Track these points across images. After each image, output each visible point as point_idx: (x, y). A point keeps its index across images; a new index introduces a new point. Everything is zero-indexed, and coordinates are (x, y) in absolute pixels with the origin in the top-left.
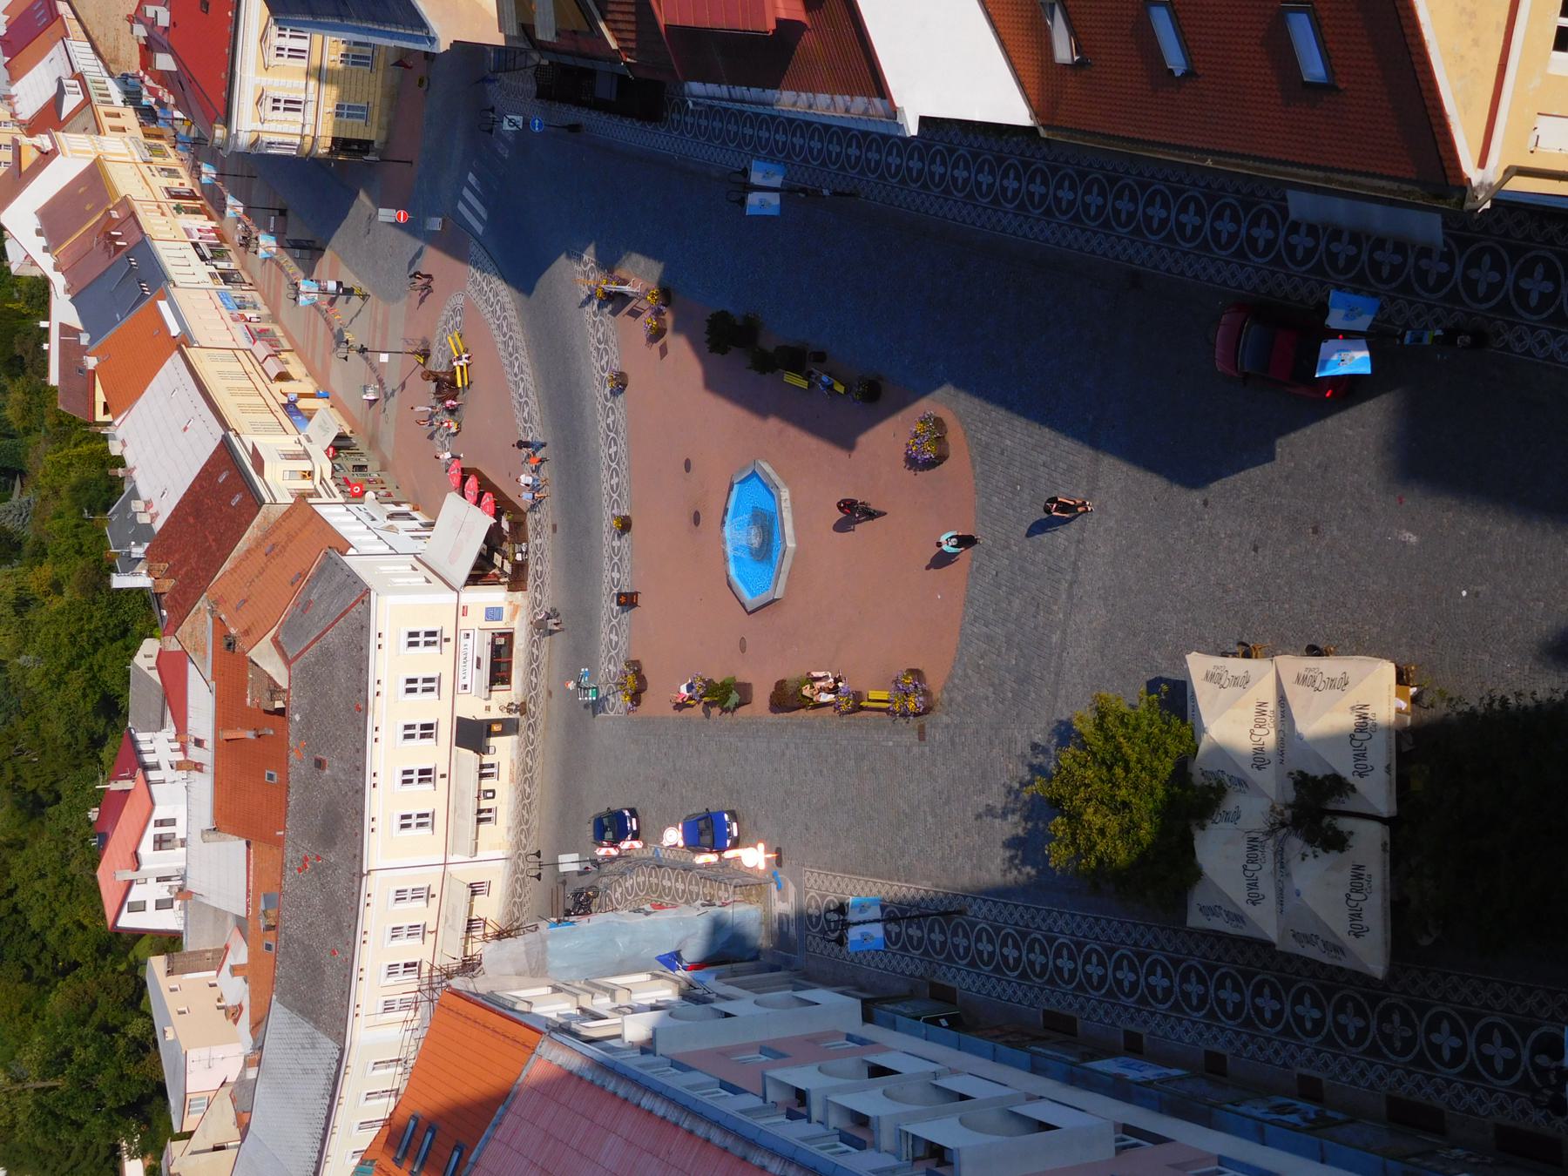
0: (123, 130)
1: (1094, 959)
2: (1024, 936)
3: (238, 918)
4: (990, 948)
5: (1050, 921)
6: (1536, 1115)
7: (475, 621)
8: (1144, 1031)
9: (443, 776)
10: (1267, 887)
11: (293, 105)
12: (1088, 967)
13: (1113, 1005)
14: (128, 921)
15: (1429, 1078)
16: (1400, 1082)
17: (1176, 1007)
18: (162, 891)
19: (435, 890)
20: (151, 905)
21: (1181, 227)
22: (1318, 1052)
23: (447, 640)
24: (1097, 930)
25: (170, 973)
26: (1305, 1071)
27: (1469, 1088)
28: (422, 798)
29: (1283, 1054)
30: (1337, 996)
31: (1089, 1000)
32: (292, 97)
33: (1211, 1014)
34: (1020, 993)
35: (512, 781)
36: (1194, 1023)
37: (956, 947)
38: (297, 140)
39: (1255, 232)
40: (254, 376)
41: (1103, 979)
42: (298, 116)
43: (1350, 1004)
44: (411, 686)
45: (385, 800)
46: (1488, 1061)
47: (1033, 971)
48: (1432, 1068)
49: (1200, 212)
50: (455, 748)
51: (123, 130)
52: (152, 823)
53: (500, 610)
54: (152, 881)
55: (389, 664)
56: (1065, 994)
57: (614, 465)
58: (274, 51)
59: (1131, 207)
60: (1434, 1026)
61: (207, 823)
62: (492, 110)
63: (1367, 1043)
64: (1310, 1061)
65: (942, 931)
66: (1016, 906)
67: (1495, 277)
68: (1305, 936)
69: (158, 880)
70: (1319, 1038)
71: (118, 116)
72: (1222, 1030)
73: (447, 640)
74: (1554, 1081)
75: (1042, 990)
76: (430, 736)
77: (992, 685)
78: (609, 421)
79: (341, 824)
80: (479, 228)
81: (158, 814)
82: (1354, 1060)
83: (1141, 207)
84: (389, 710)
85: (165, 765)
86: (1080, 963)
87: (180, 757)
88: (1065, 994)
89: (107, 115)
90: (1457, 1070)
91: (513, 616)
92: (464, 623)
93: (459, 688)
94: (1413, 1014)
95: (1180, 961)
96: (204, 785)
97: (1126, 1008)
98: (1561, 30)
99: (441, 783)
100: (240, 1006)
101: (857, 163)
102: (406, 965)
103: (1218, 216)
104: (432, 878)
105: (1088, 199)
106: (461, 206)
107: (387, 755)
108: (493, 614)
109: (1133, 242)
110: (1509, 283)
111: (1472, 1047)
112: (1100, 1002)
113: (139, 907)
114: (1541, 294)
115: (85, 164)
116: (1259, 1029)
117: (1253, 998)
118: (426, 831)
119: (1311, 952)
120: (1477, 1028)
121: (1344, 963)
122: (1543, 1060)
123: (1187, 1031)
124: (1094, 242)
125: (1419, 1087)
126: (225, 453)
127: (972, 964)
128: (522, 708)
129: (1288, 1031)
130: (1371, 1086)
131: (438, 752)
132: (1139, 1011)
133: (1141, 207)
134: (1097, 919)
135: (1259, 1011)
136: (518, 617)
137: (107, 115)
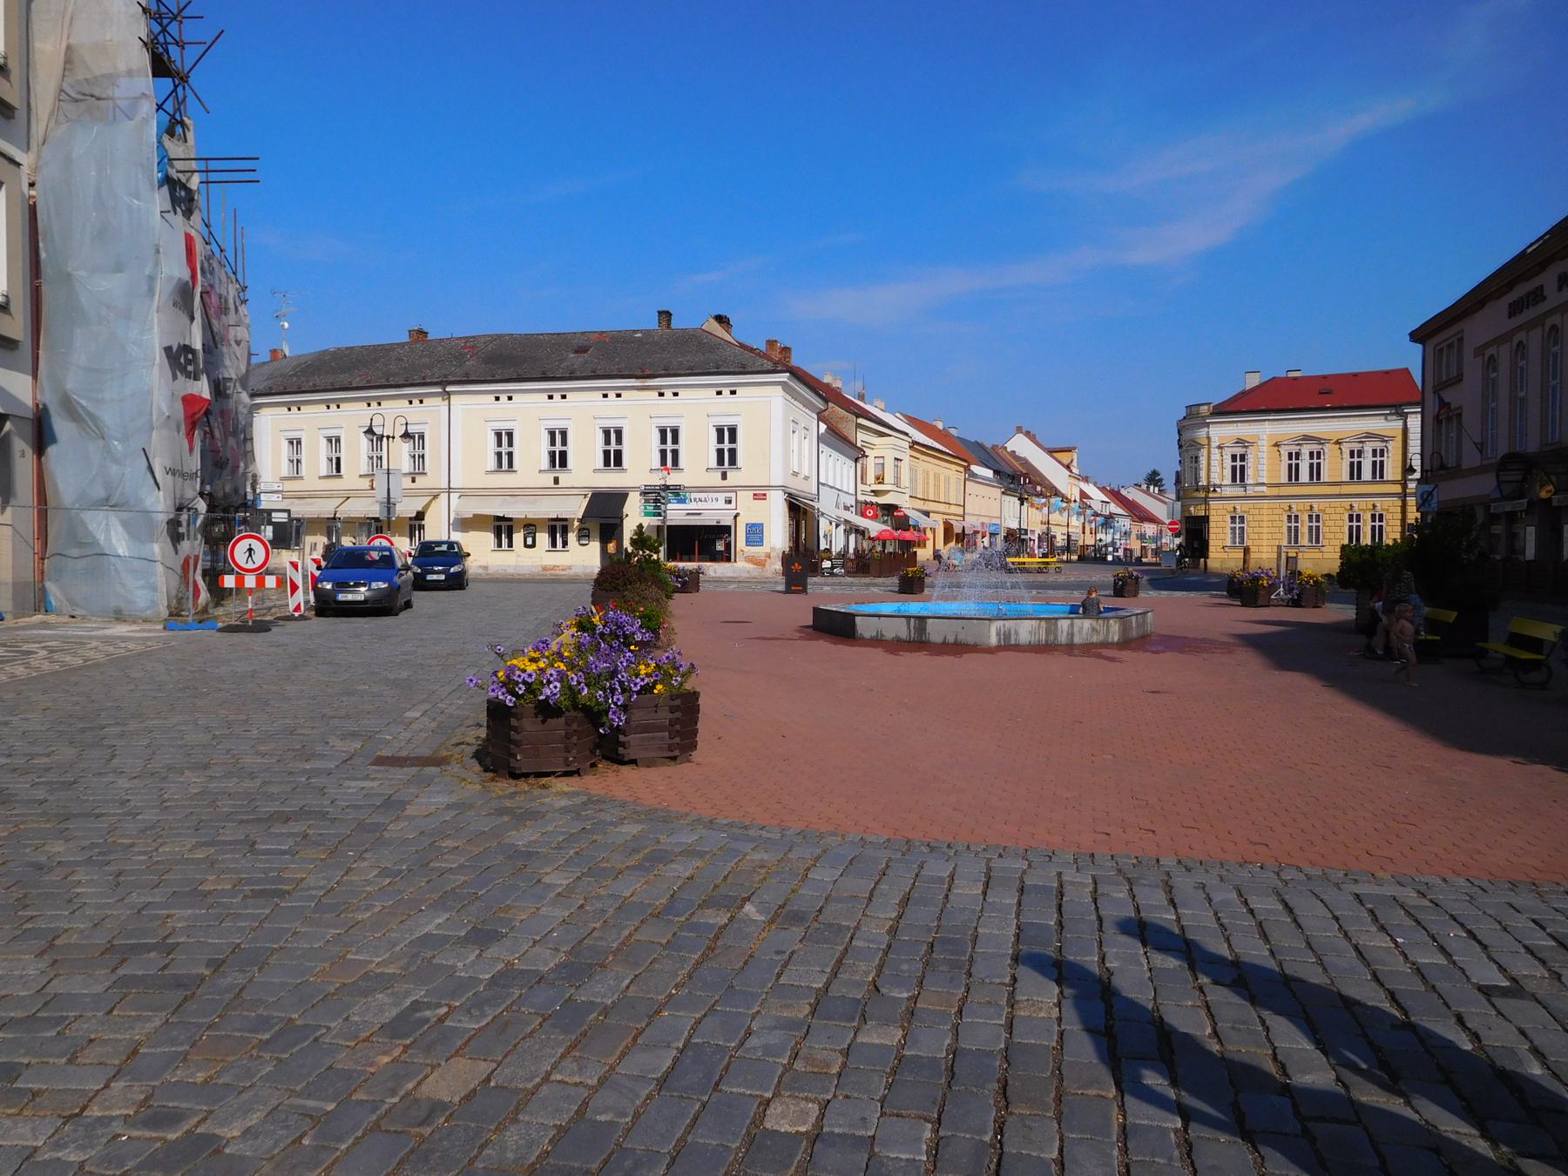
7: (749, 510)
9: (556, 481)
23: (724, 476)
28: (532, 453)
32: (1249, 472)
35: (545, 568)
38: (1203, 482)
42: (1228, 481)
44: (670, 435)
53: (760, 542)
58: (1294, 449)
73: (724, 476)
76: (607, 463)
77: (578, 969)
91: (751, 560)
92: (745, 497)
99: (548, 480)
102: (338, 459)
104: (435, 476)
108: (756, 533)
118: (491, 463)
131: (586, 471)
136: (750, 566)
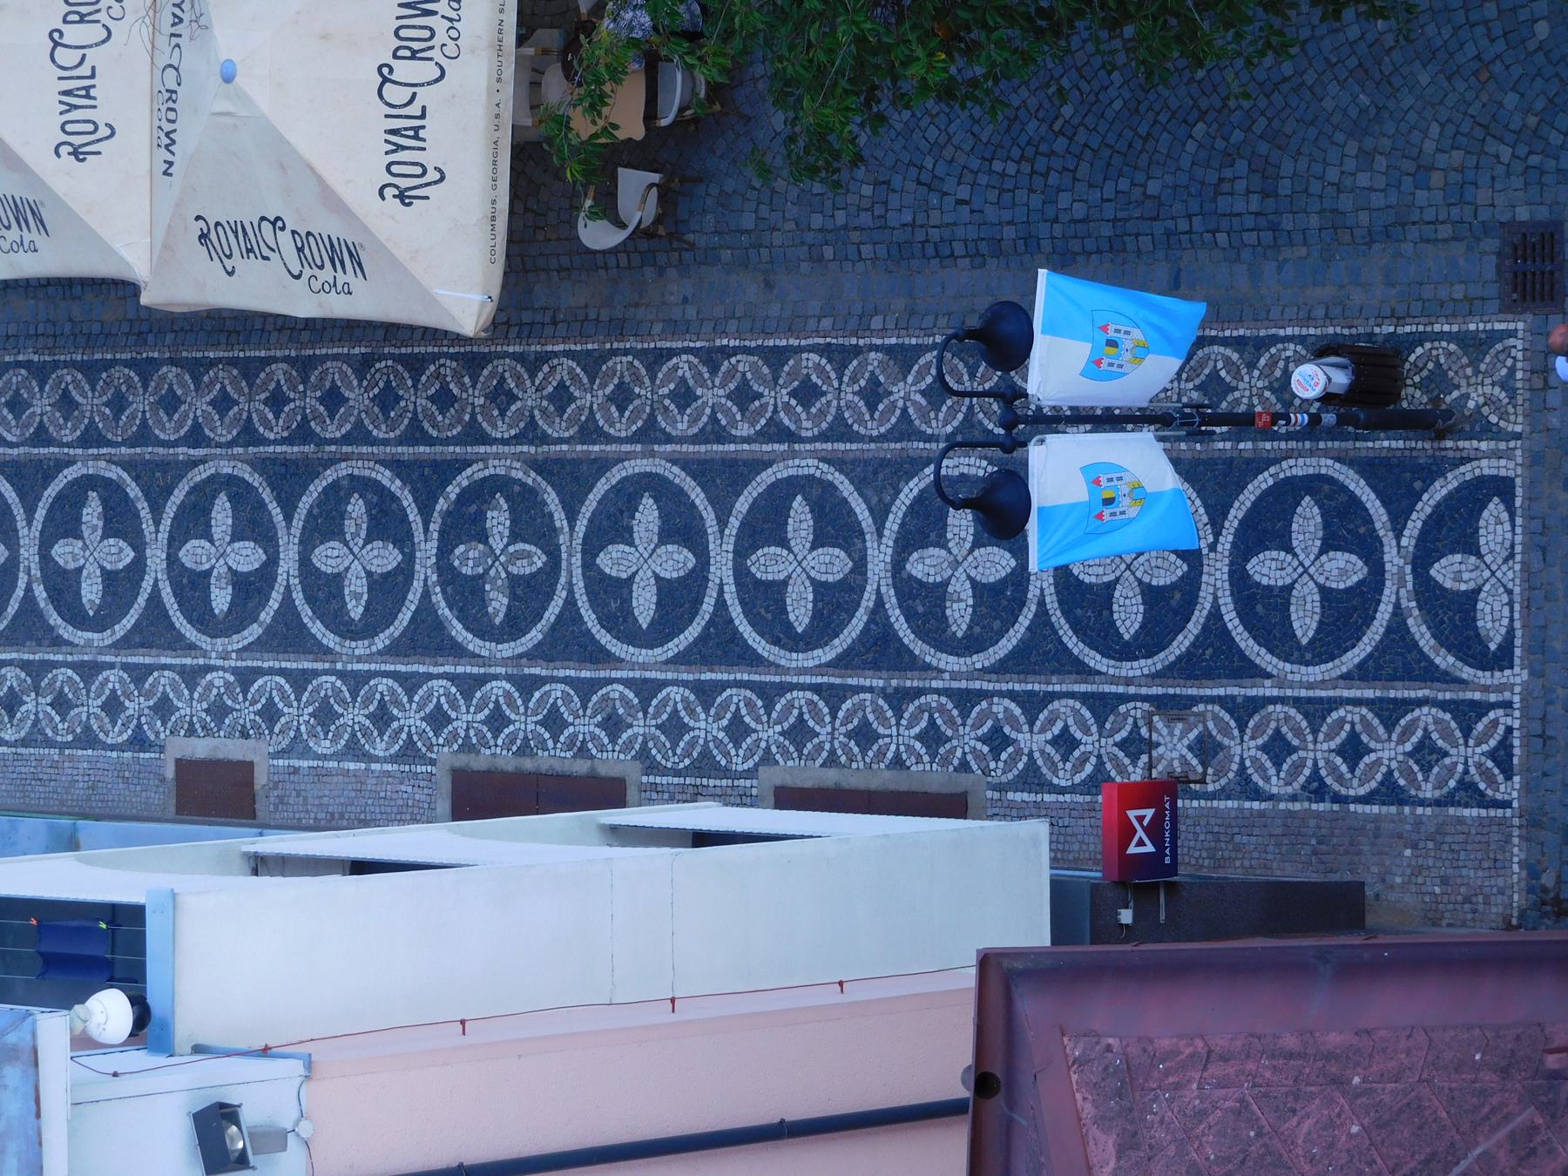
10: (124, 96)
15: (586, 689)
16: (497, 721)
22: (246, 678)
26: (200, 748)
27: (706, 693)
30: (316, 488)
48: (601, 656)
64: (219, 711)
68: (238, 229)
70: (254, 632)
94: (552, 499)
110: (879, 557)
116: (58, 642)
119: (263, 288)
121: (364, 301)
125: (554, 722)
130: (409, 753)
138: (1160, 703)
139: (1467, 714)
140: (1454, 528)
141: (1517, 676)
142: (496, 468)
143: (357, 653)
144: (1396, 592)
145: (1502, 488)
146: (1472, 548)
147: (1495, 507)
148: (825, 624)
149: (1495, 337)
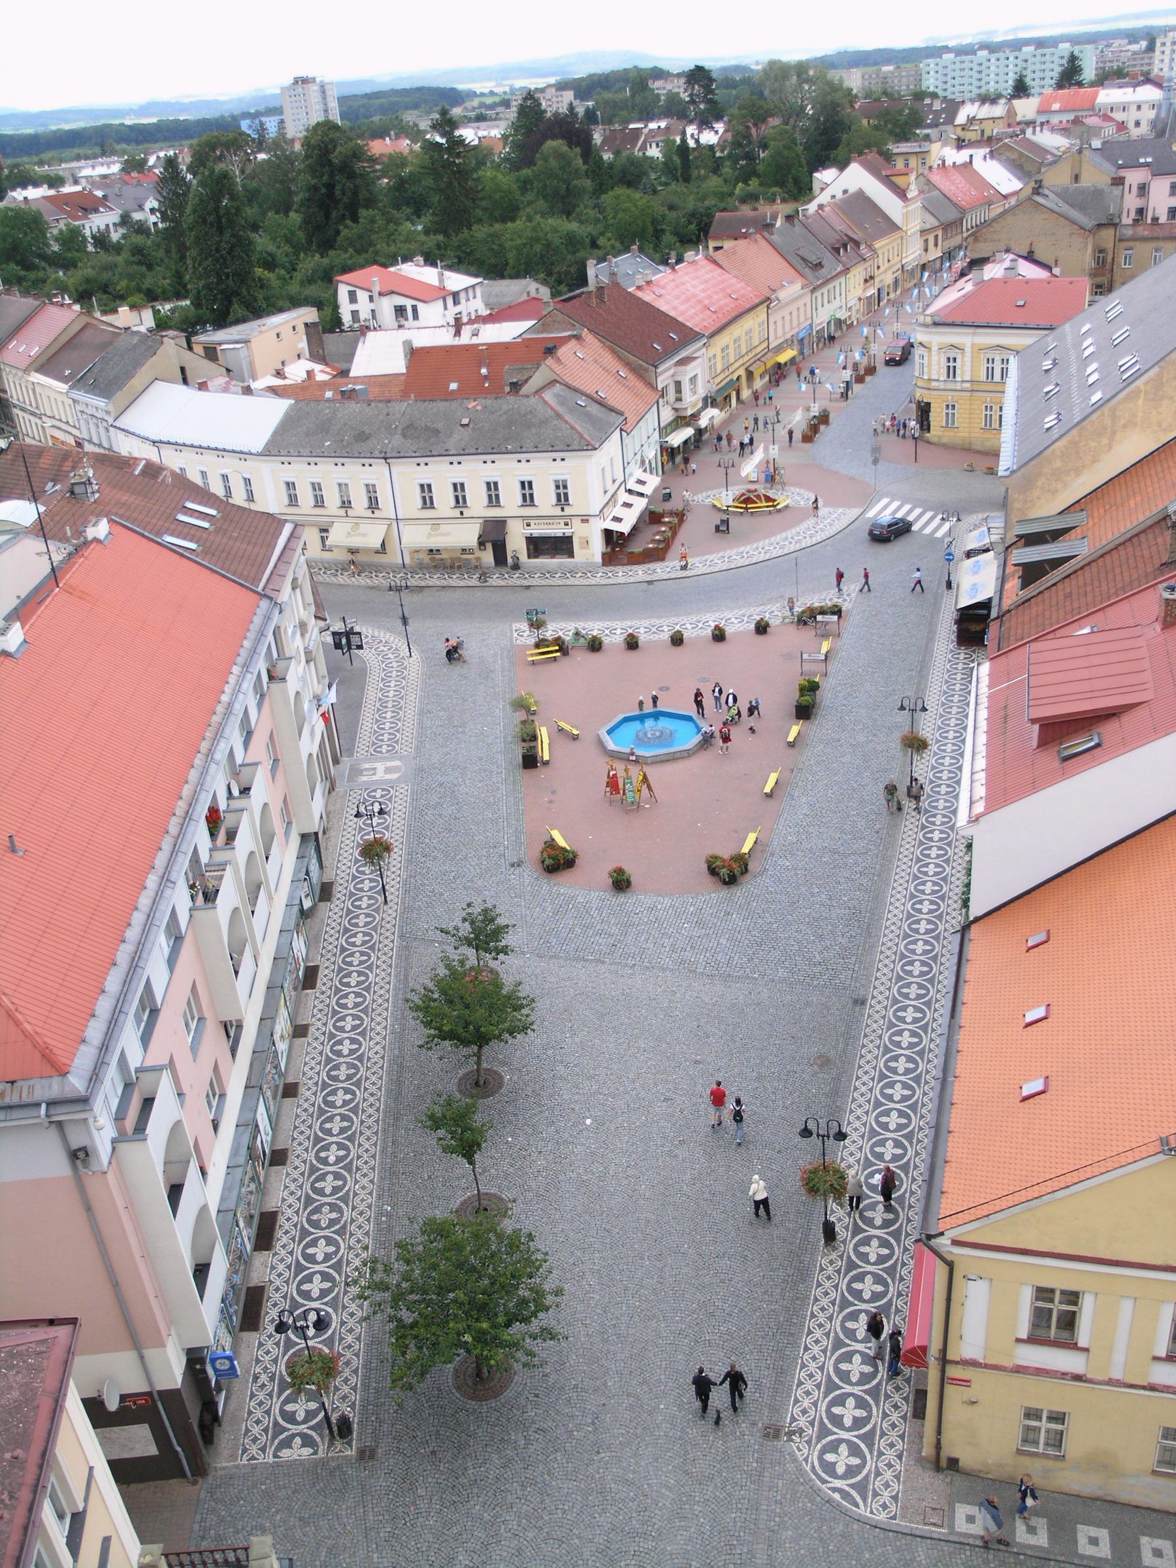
0: (926, 250)
1: (359, 1000)
2: (372, 948)
3: (348, 371)
4: (361, 924)
5: (384, 967)
6: (274, 1313)
8: (310, 1039)
9: (462, 513)
11: (951, 372)
12: (353, 995)
13: (327, 1015)
14: (343, 292)
15: (293, 1239)
17: (329, 1060)
18: (364, 315)
19: (377, 513)
20: (354, 307)
21: (900, 1033)
22: (305, 1162)
23: (563, 509)
24: (380, 1001)
25: (306, 325)
28: (444, 499)
29: (302, 1137)
31: (329, 997)
32: (958, 371)
33: (325, 1085)
34: (330, 947)
36: (318, 1073)
37: (360, 899)
39: (898, 1086)
40: (750, 355)
41: (345, 1006)
43: (340, 1183)
44: (527, 485)
45: (441, 474)
46: (309, 1279)
47: (347, 956)
48: (300, 1242)
49: (911, 1046)
50: (481, 521)
51: (926, 250)
52: (415, 303)
54: (372, 306)
55: (543, 471)
56: (331, 980)
57: (700, 625)
59: (912, 996)
60: (330, 1241)
61: (417, 344)
62: (959, 520)
63: (314, 1196)
65: (371, 888)
66: (393, 941)
67: (873, 1258)
69: (373, 311)
70: (315, 1162)
71: (936, 245)
72: (315, 1094)
73: (563, 509)
74: (298, 1324)
75: (334, 963)
78: (733, 620)
79: (425, 442)
80: (871, 514)
81: (421, 307)
82: (301, 1187)
83: (913, 1003)
84: (508, 471)
85: (458, 309)
86: (355, 989)
87: (465, 319)
88: (331, 980)
89: (936, 237)
90: (300, 1258)
93: (527, 521)
95: (361, 1061)
96: (445, 338)
97: (325, 1025)
98: (1165, 1449)
99: (457, 513)
100: (285, 378)
101: (935, 792)
103: (909, 1059)
105: (917, 964)
106: (885, 501)
107: (474, 473)
109: (887, 998)
111: (317, 1268)
112: (328, 1006)
113: (353, 298)
114: (861, 1291)
115: (900, 225)
117: (339, 1114)
120: (331, 1271)
122: (313, 1317)
123: (312, 1069)
124: (885, 970)
126: (689, 336)
127: (349, 912)
128: (516, 567)
129: (318, 1140)
130: (284, 1200)
132: (324, 1034)
133: (913, 1003)
134: (387, 1000)
135: (330, 1119)
137: (936, 237)
138: (274, 1374)
139: (263, 1449)
140: (307, 1441)
141: (271, 1460)
142: (346, 1214)
143: (867, 1149)
144: (848, 1389)
145: (315, 1453)
146: (302, 1446)
147: (311, 1451)
148: (302, 1293)
149: (351, 1446)
